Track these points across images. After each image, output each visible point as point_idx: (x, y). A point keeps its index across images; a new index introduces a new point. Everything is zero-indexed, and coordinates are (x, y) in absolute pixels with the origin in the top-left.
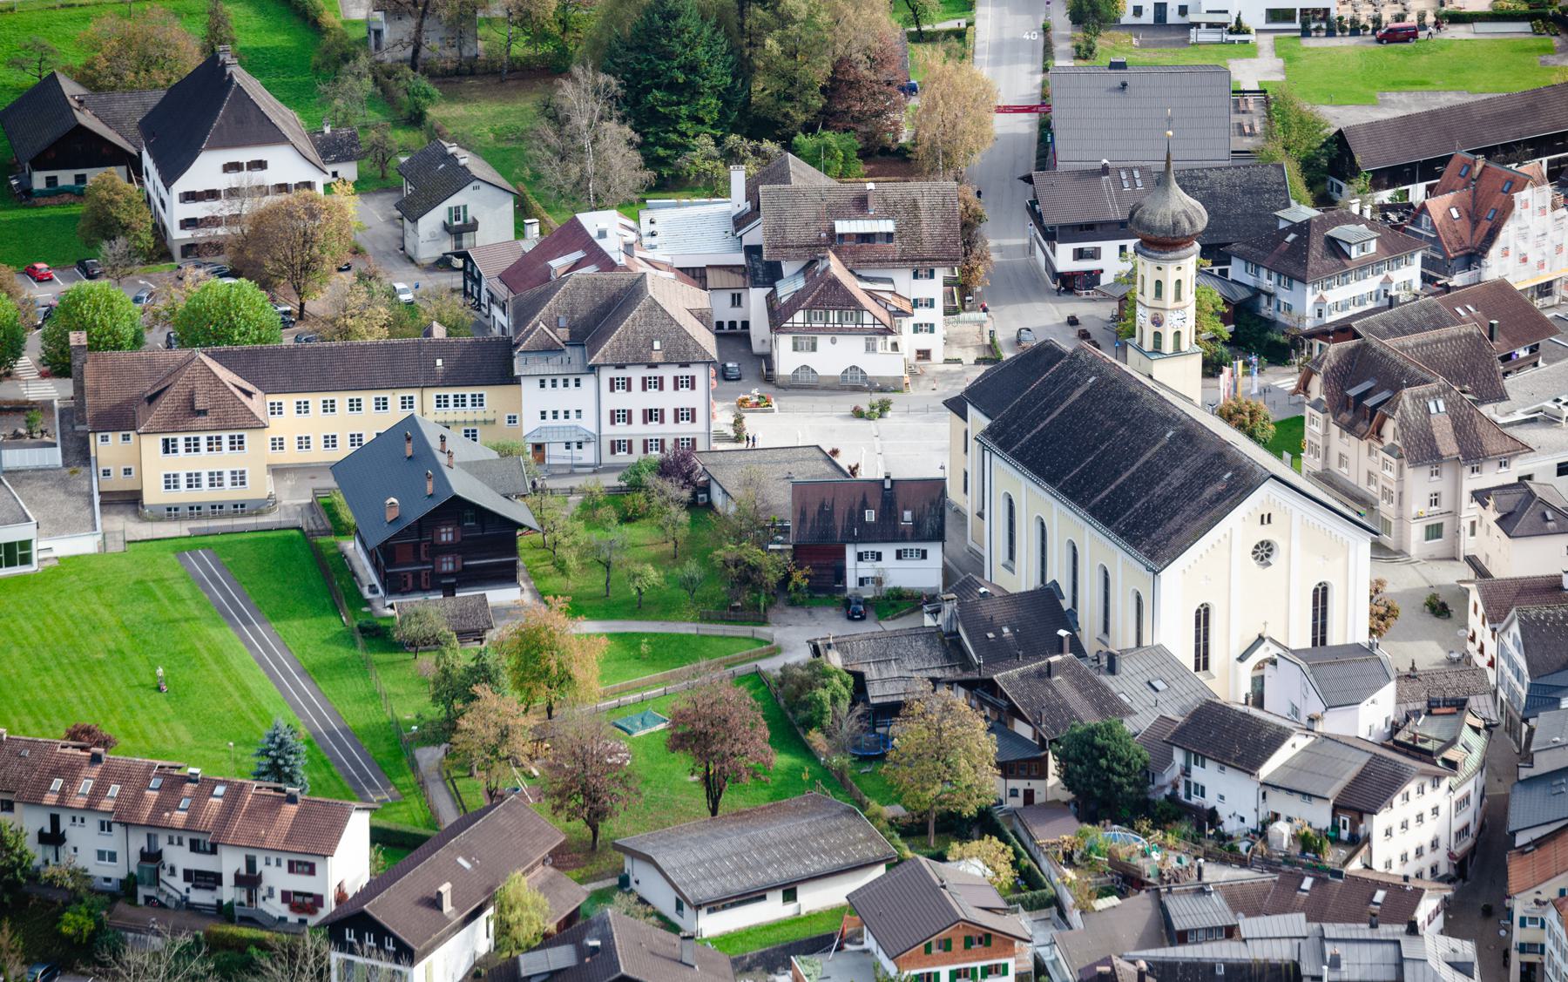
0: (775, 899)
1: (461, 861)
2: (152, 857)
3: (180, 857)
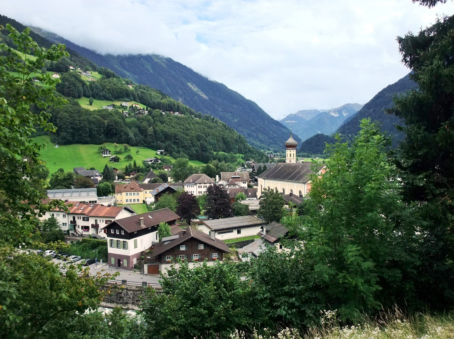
0: (235, 232)
1: (149, 216)
2: (74, 222)
3: (80, 223)
